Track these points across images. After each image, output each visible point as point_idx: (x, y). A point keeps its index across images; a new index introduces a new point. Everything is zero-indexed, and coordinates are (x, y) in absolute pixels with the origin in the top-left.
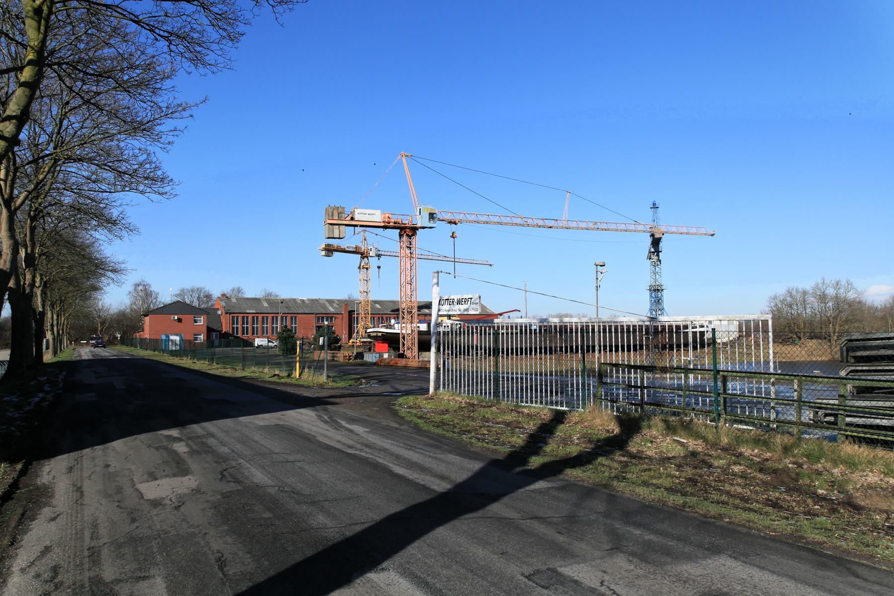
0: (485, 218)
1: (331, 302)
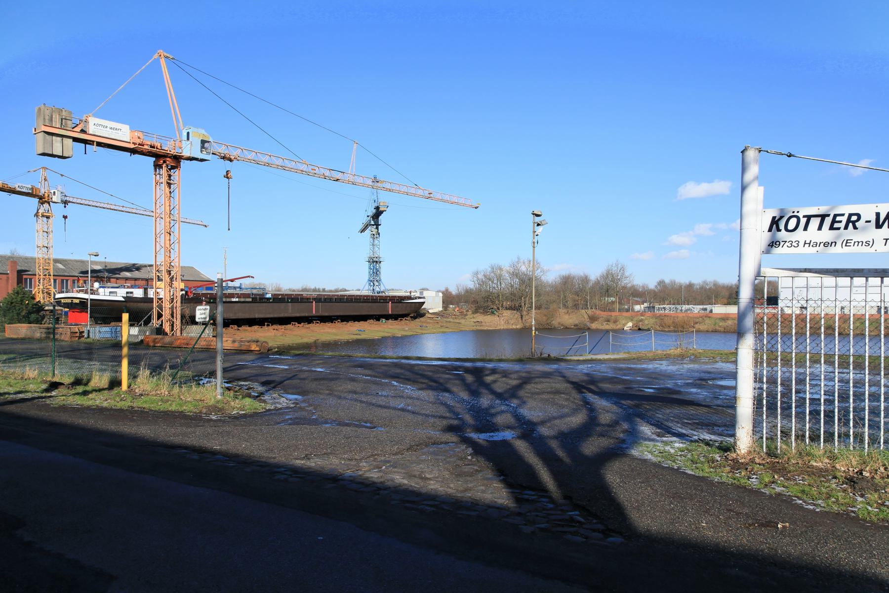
0: (266, 159)
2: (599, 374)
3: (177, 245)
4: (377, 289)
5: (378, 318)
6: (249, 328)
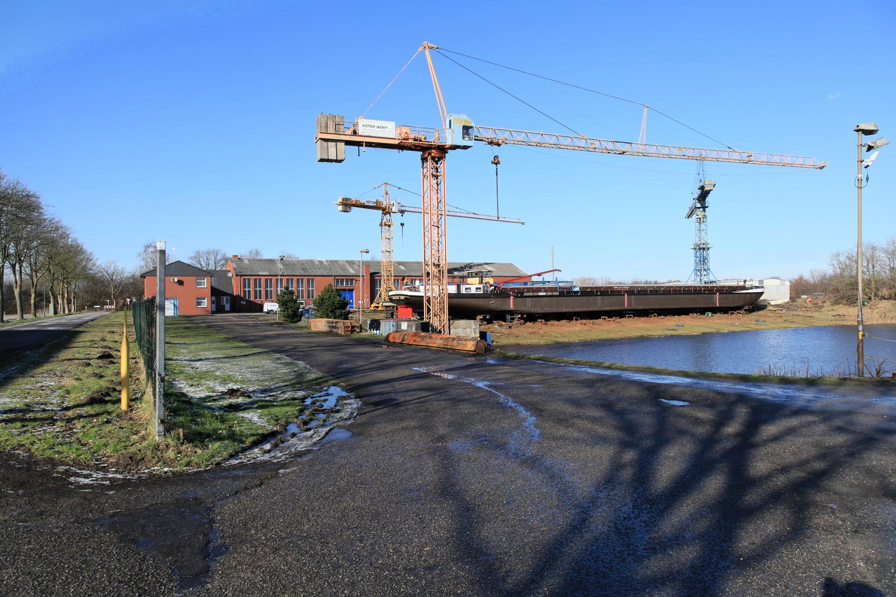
0: (537, 139)
1: (351, 263)
3: (443, 237)
4: (706, 279)
5: (702, 311)
6: (556, 322)
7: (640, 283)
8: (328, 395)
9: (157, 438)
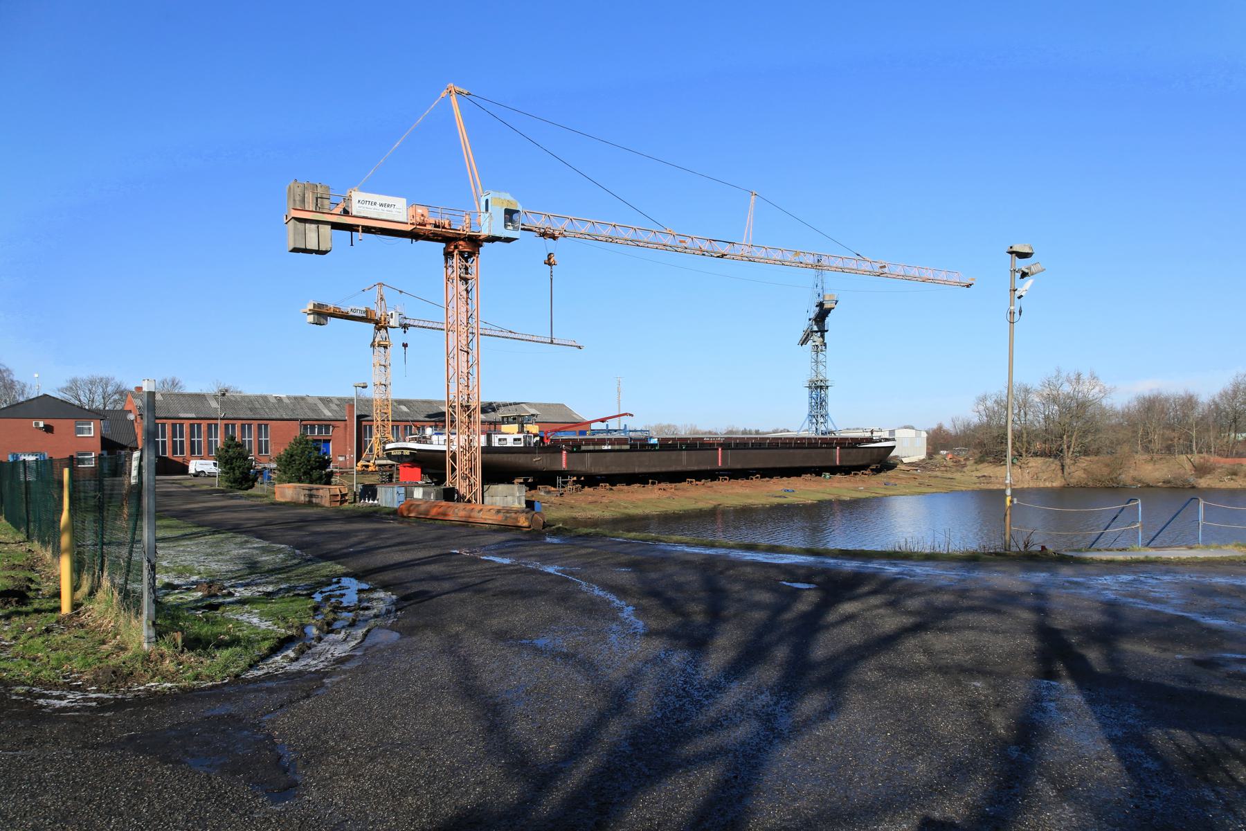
0: (608, 231)
1: (326, 401)
2: (1141, 604)
3: (475, 367)
4: (823, 428)
5: (818, 471)
6: (626, 488)
7: (736, 433)
8: (342, 588)
9: (146, 646)
